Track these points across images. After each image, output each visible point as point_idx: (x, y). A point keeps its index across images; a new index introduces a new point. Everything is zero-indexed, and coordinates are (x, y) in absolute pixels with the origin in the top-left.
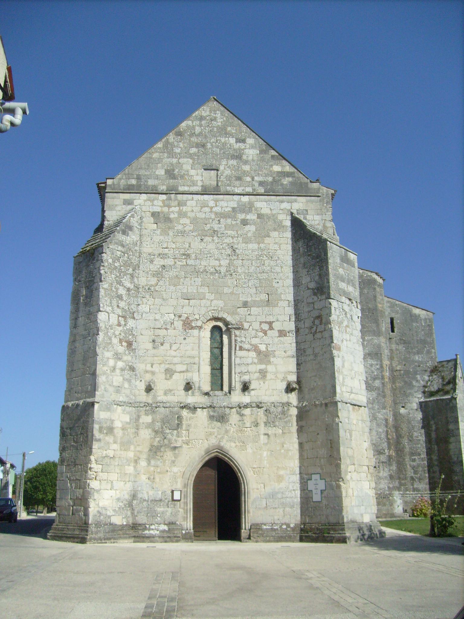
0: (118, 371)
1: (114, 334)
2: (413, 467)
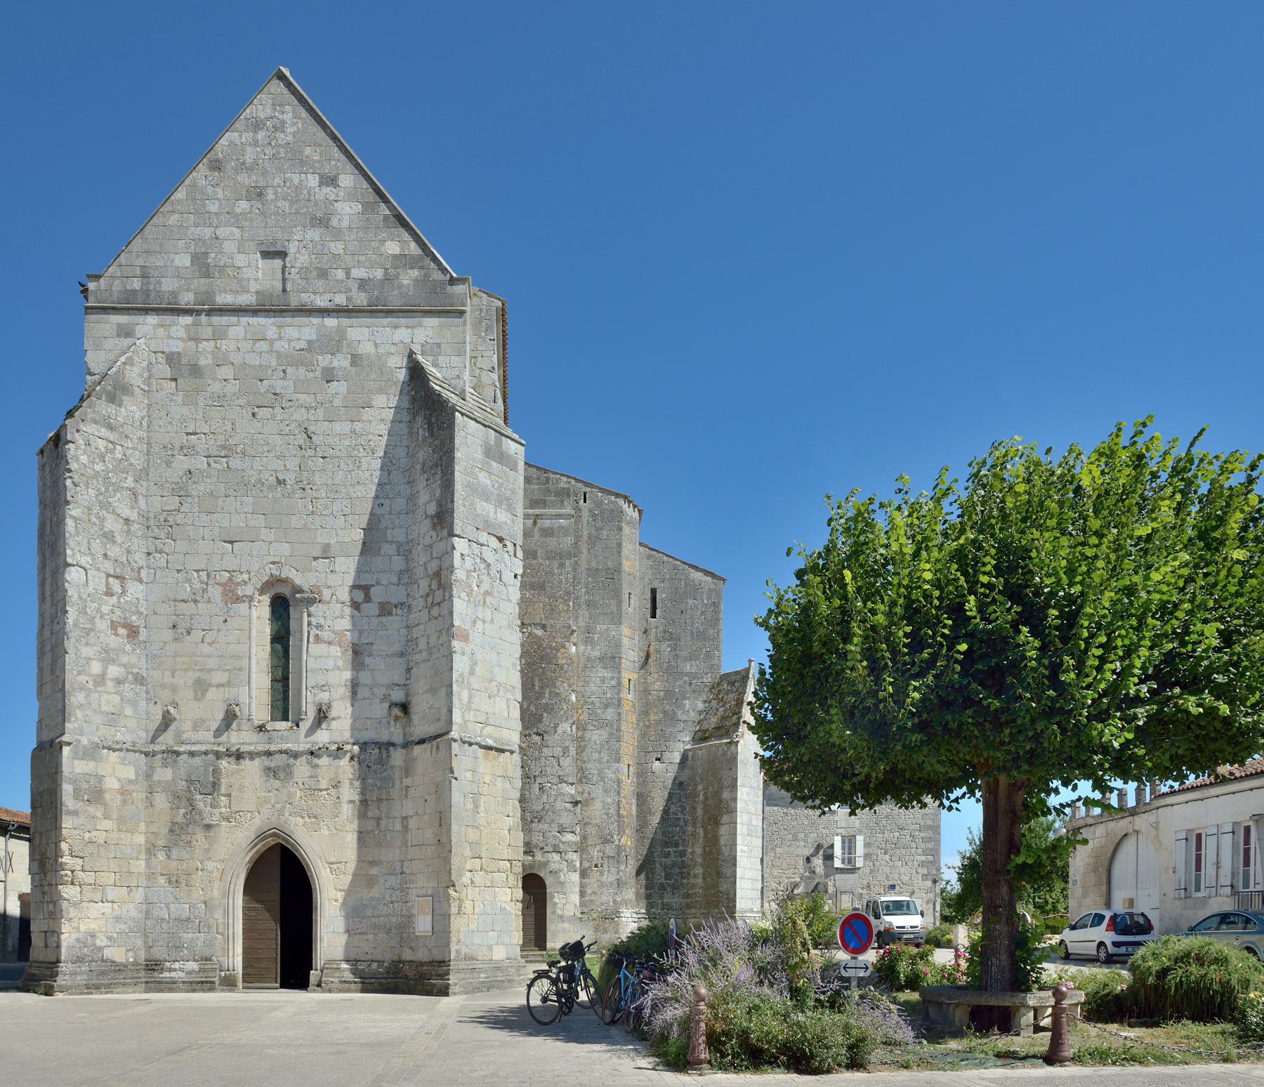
0: (110, 685)
1: (98, 610)
2: (665, 868)
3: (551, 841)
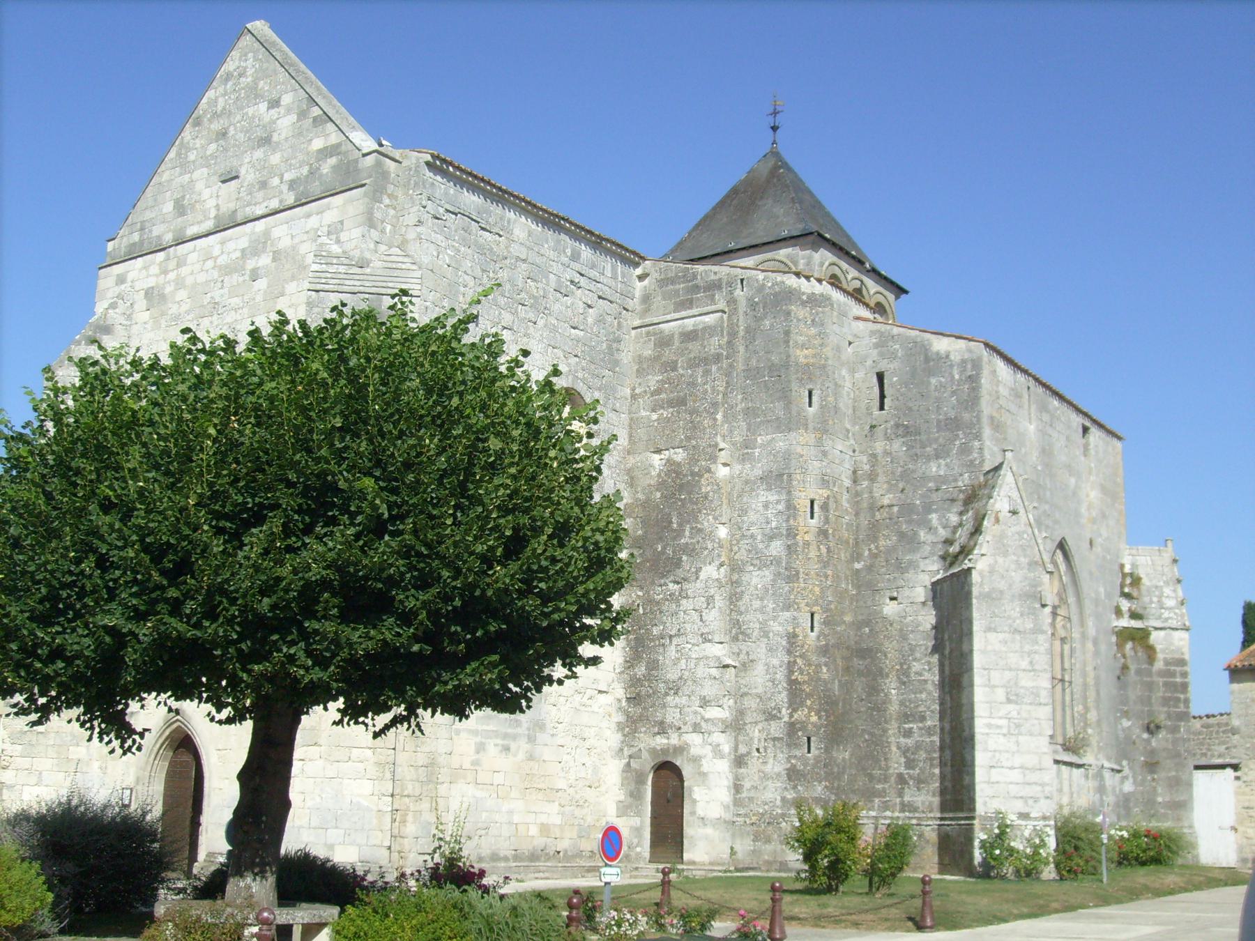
2: (905, 751)
3: (691, 719)
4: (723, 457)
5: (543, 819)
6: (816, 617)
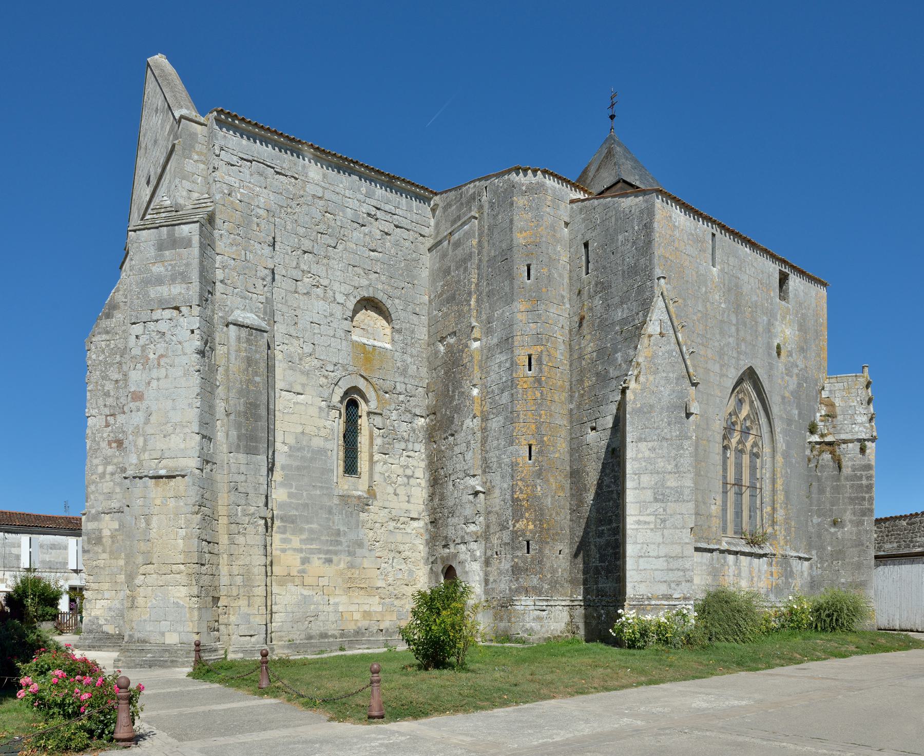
1: (102, 437)
4: (476, 333)
5: (366, 608)
6: (533, 448)
